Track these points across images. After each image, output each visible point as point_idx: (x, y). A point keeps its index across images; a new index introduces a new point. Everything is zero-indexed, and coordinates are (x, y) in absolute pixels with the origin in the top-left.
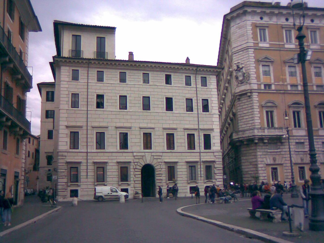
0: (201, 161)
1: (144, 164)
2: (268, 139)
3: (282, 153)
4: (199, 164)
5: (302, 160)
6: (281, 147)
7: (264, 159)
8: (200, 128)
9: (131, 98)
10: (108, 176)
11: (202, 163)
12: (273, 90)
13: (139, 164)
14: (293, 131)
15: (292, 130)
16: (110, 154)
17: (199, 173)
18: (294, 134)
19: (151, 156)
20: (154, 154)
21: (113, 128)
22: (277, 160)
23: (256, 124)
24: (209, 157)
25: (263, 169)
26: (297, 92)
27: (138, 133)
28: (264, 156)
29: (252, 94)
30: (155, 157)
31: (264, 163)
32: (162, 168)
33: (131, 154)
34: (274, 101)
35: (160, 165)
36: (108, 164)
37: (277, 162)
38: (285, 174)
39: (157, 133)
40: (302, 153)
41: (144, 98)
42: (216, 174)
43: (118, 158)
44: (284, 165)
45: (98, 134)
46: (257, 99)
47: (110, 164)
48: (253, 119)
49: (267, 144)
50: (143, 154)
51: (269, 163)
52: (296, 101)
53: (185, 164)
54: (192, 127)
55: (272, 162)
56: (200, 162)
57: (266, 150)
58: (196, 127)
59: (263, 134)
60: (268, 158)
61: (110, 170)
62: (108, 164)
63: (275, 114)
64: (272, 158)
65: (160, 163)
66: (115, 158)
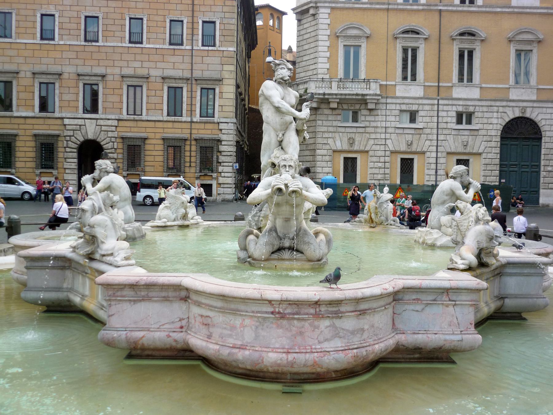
0: (192, 139)
1: (82, 139)
2: (338, 100)
3: (368, 130)
4: (188, 143)
5: (410, 145)
6: (369, 118)
7: (330, 141)
8: (194, 76)
9: (107, 22)
10: (17, 159)
11: (193, 143)
12: (479, 7)
13: (73, 139)
14: (398, 87)
15: (396, 85)
16: (22, 121)
17: (187, 159)
18: (398, 94)
19: (97, 125)
20: (101, 122)
21: (29, 75)
22: (356, 143)
23: (320, 71)
24: (209, 132)
25: (327, 158)
26: (507, 10)
27: (72, 83)
28: (330, 135)
29: (318, 10)
30: (104, 128)
31: (329, 148)
32: (115, 147)
33: (59, 122)
34: (362, 26)
35: (113, 142)
36: (17, 137)
37: (356, 148)
38: (370, 171)
39: (23, 82)
40: (412, 131)
41: (205, 24)
42: (220, 163)
43: (36, 127)
44: (371, 153)
45: (44, 86)
46: (328, 21)
47: (21, 138)
48: (315, 61)
49: (337, 112)
50: (80, 122)
51: (339, 148)
52: (413, 26)
53: (161, 142)
54: (178, 73)
55: (346, 147)
56: (191, 140)
57: (335, 123)
58: (187, 75)
59: (327, 91)
60: (338, 138)
61: (21, 149)
62: (17, 138)
63: (363, 52)
64: (345, 139)
65: (113, 140)
66: (31, 127)
